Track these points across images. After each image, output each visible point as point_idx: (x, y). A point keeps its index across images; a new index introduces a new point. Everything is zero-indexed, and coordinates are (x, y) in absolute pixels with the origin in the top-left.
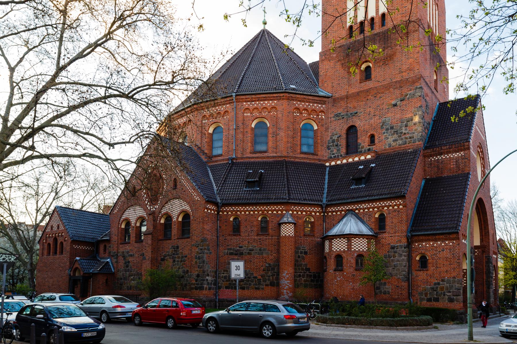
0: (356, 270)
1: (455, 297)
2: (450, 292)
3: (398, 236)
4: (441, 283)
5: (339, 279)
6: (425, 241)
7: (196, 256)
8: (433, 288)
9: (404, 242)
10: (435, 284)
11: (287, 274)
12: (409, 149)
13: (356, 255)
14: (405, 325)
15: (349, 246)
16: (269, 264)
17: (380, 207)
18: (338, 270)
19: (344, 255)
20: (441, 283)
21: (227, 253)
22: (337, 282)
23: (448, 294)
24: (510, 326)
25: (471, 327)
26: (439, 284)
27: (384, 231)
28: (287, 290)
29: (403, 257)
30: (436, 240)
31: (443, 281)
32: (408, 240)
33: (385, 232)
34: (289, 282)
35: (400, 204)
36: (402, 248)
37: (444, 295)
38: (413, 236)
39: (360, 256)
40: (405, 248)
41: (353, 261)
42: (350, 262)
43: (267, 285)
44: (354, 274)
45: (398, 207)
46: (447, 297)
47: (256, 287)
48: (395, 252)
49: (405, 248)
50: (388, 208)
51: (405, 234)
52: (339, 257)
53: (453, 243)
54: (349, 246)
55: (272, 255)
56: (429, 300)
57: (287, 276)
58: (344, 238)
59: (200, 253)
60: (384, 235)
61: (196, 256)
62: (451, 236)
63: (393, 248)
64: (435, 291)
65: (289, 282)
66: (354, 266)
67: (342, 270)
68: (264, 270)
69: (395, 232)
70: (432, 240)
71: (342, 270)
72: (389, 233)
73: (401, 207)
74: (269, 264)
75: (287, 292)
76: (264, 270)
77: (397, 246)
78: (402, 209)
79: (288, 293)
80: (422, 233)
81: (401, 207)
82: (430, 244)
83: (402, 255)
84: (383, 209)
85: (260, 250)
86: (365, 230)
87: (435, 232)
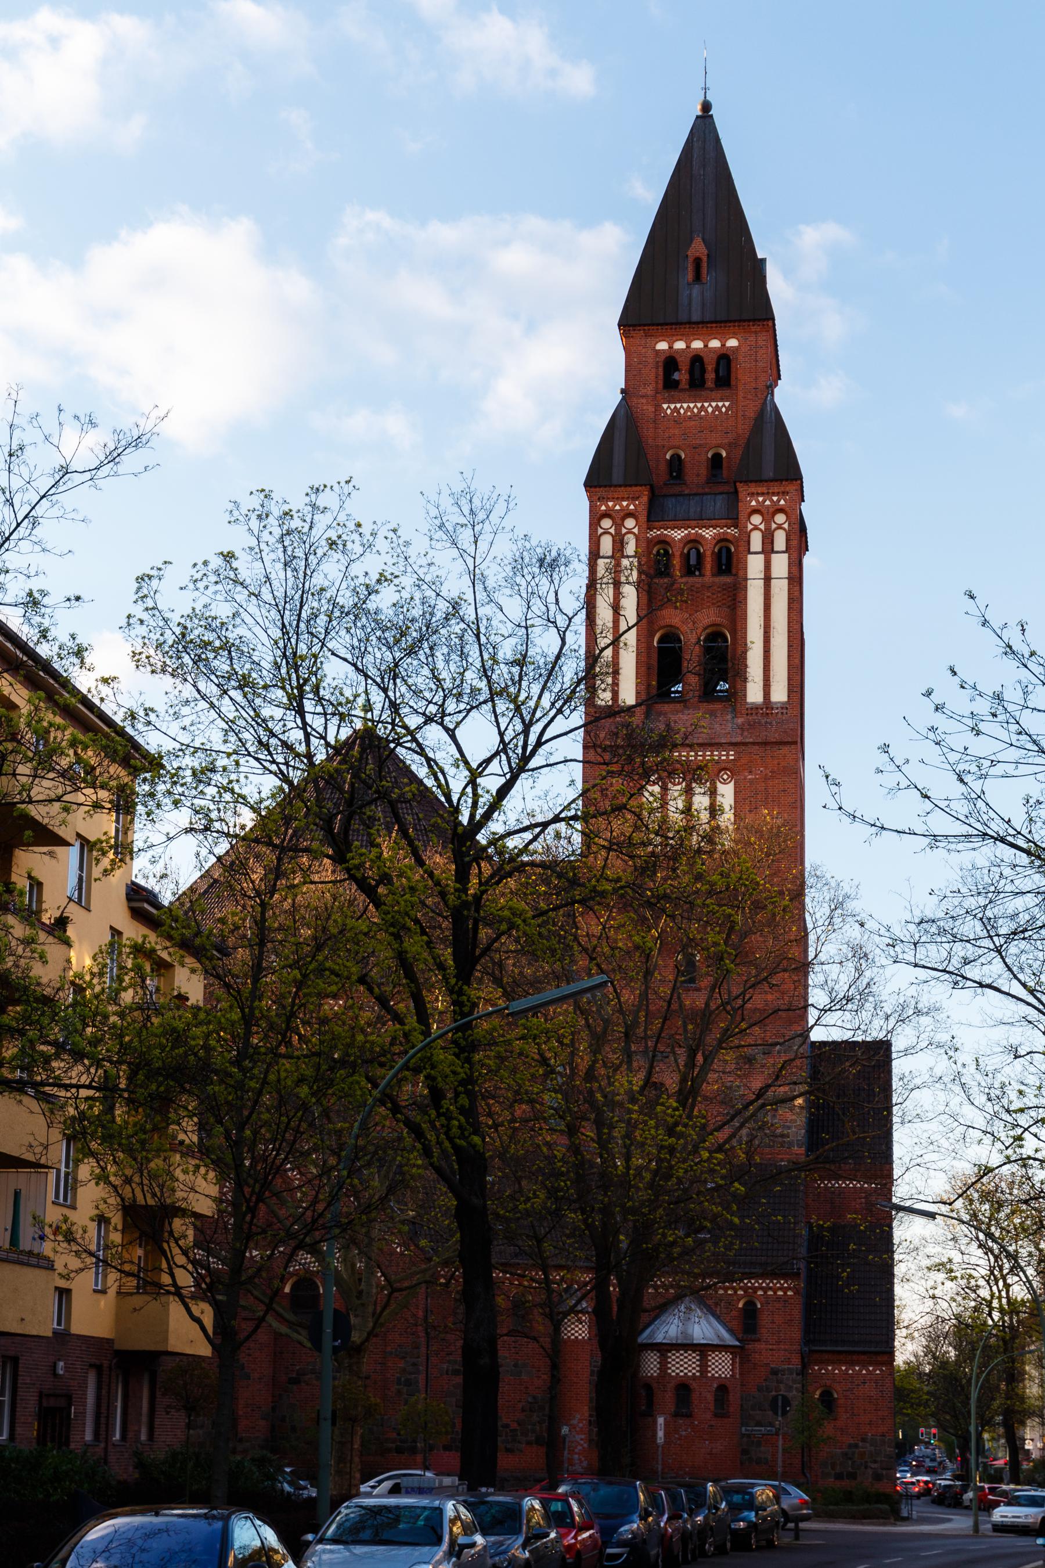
0: (716, 1415)
1: (884, 1472)
2: (875, 1462)
3: (785, 1350)
4: (860, 1444)
5: (684, 1433)
6: (832, 1363)
7: (399, 1379)
8: (846, 1454)
9: (796, 1363)
10: (850, 1446)
11: (581, 1420)
12: (782, 1160)
13: (715, 1385)
14: (869, 1518)
15: (704, 1366)
16: (534, 1398)
17: (750, 1288)
18: (682, 1416)
19: (694, 1385)
20: (860, 1444)
21: (447, 1371)
22: (679, 1439)
23: (873, 1466)
24: (1006, 1517)
25: (976, 1516)
26: (856, 1446)
27: (753, 1337)
28: (579, 1454)
29: (794, 1392)
30: (851, 1364)
31: (864, 1440)
32: (803, 1358)
33: (759, 1340)
34: (583, 1437)
35: (789, 1288)
36: (792, 1374)
37: (866, 1468)
38: (811, 1351)
39: (722, 1388)
40: (798, 1374)
41: (710, 1397)
42: (704, 1399)
43: (529, 1443)
44: (712, 1423)
45: (785, 1293)
46: (870, 1471)
47: (509, 1446)
48: (779, 1382)
49: (798, 1374)
50: (765, 1292)
51: (796, 1347)
52: (684, 1388)
53: (881, 1370)
54: (704, 1366)
55: (539, 1377)
56: (839, 1477)
57: (581, 1425)
58: (694, 1352)
59: (410, 1373)
60: (757, 1345)
61: (399, 1379)
62: (879, 1358)
63: (775, 1372)
64: (850, 1459)
65: (583, 1437)
66: (712, 1406)
67: (689, 1416)
68: (523, 1410)
69: (778, 1343)
70: (845, 1363)
71: (689, 1416)
72: (767, 1342)
73: (790, 1293)
74: (534, 1398)
75: (580, 1459)
76: (523, 1410)
77: (783, 1370)
78: (791, 1297)
79: (581, 1462)
80: (829, 1348)
81: (790, 1293)
82: (840, 1370)
83: (791, 1387)
84: (755, 1292)
85: (515, 1365)
86: (729, 1339)
87: (851, 1349)
